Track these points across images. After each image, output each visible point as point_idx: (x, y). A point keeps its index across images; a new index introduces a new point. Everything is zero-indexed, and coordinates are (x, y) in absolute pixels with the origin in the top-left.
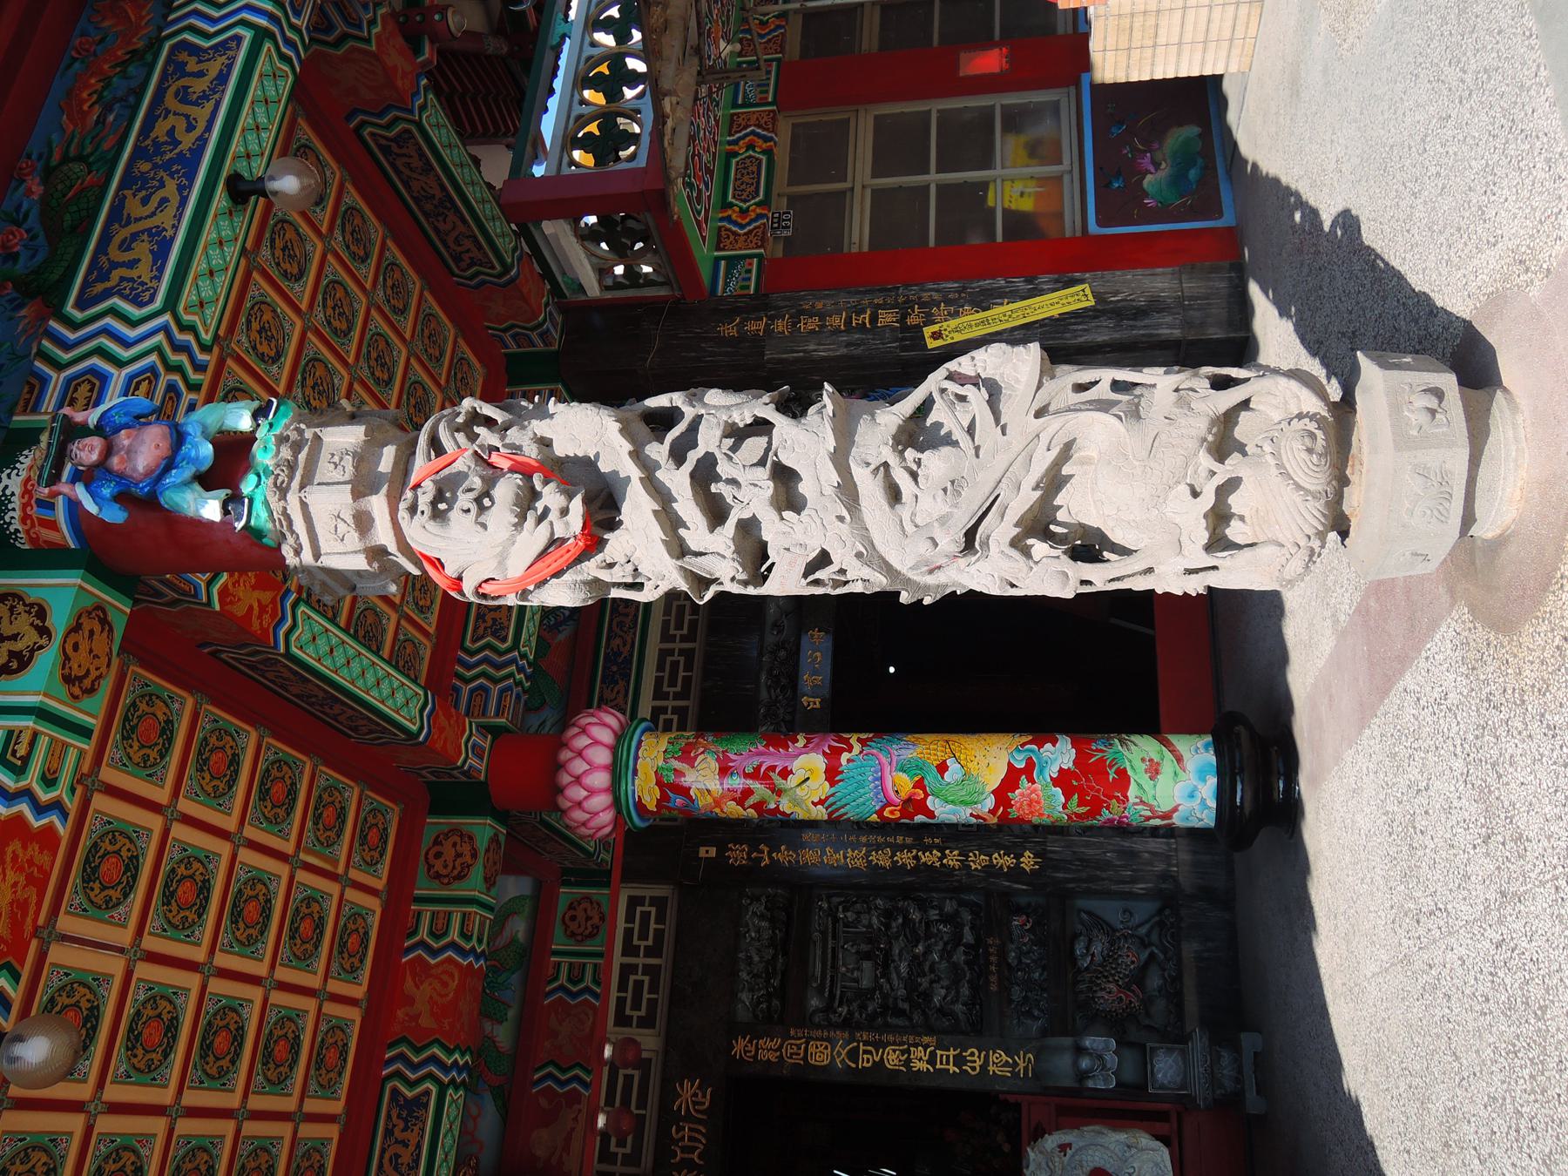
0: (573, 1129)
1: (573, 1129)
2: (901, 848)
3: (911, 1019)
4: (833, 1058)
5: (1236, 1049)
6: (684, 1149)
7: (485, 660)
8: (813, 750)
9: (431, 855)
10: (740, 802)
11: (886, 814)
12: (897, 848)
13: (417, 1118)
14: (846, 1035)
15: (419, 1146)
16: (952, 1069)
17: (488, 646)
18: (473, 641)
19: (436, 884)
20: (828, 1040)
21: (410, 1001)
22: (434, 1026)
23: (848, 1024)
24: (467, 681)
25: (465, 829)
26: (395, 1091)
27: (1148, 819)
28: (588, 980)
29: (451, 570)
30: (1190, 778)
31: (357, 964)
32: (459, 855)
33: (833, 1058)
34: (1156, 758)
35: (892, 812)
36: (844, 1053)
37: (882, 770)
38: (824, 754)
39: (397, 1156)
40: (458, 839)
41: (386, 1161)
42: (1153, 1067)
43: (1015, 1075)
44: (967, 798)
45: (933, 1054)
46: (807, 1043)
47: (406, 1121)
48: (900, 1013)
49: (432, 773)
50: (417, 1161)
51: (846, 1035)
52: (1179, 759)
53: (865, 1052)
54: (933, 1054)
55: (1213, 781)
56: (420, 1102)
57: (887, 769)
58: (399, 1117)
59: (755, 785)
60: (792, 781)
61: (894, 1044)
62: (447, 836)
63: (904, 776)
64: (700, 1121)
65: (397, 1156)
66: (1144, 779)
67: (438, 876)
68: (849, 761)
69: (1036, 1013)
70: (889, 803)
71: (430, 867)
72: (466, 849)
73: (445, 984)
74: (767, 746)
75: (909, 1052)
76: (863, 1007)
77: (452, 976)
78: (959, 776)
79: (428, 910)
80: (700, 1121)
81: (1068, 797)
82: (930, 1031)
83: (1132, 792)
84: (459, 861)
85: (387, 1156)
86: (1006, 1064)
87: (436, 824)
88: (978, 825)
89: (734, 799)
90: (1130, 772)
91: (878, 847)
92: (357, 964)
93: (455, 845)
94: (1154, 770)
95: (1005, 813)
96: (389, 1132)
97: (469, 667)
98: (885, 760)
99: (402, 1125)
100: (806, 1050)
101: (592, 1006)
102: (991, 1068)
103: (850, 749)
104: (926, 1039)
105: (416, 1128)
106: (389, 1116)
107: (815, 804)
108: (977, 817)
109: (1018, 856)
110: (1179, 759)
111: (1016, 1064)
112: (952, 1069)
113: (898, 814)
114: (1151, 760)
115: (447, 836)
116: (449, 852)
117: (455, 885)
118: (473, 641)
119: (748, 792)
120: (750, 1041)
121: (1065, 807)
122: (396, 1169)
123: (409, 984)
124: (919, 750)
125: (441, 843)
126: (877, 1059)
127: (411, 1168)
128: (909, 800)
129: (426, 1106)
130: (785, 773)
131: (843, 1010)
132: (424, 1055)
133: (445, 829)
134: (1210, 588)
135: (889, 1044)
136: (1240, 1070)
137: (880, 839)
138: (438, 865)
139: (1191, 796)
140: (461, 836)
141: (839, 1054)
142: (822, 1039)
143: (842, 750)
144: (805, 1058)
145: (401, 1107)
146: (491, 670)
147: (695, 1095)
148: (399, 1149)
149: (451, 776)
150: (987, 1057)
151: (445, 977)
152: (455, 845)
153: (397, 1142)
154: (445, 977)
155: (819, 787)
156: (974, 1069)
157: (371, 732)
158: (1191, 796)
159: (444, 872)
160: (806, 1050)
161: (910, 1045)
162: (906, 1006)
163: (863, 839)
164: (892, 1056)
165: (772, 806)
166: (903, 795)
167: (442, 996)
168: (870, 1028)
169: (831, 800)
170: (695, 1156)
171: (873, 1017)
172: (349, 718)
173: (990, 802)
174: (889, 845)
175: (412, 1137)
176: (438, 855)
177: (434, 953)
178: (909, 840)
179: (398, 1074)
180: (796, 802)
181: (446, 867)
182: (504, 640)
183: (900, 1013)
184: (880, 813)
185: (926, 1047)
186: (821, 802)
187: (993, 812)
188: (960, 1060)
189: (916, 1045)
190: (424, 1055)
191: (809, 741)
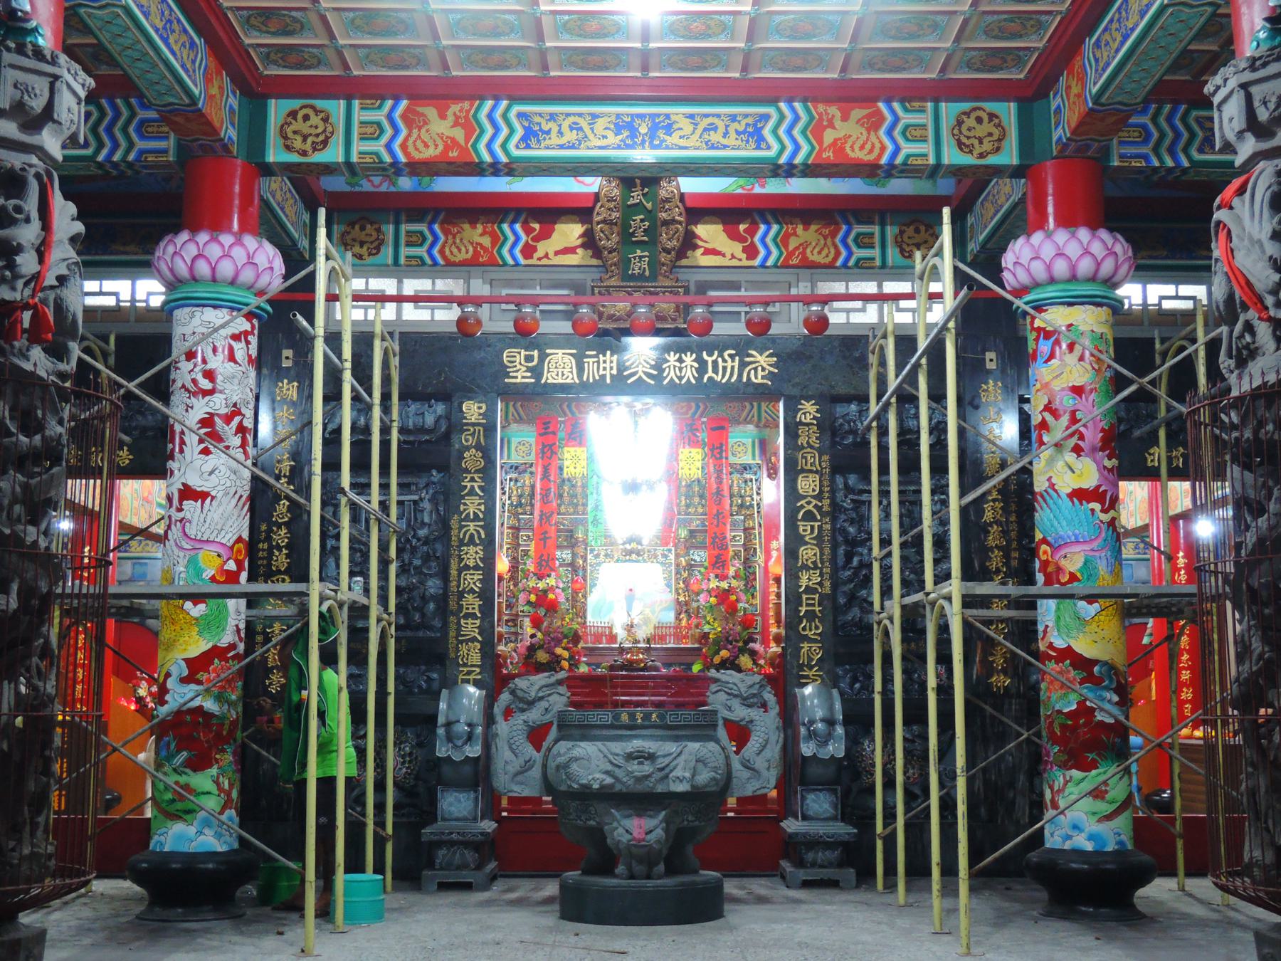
0: (724, 255)
1: (724, 255)
2: (1007, 556)
3: (844, 568)
4: (805, 497)
5: (841, 864)
6: (715, 363)
7: (1178, 135)
8: (1101, 474)
9: (979, 113)
10: (1048, 408)
11: (1044, 547)
12: (1006, 551)
13: (747, 141)
14: (826, 509)
15: (725, 147)
16: (803, 609)
17: (1193, 135)
18: (1197, 120)
19: (953, 122)
20: (821, 492)
21: (845, 118)
22: (825, 145)
23: (836, 508)
24: (1154, 119)
25: (1005, 143)
26: (766, 117)
27: (1051, 787)
28: (859, 253)
29: (1236, 202)
30: (1093, 826)
31: (877, 67)
32: (981, 141)
33: (805, 497)
34: (1108, 797)
35: (1045, 552)
36: (810, 507)
37: (1085, 542)
38: (1098, 487)
39: (715, 129)
40: (995, 137)
41: (710, 120)
42: (820, 790)
43: (801, 667)
44: (1062, 623)
45: (814, 591)
46: (816, 472)
47: (744, 132)
48: (849, 556)
49: (1059, 107)
50: (713, 147)
51: (826, 509)
52: (1109, 817)
53: (812, 527)
54: (814, 591)
55: (1089, 847)
56: (760, 141)
57: (1087, 547)
58: (747, 125)
59: (1065, 420)
60: (1070, 457)
61: (822, 554)
62: (999, 125)
63: (1080, 564)
64: (740, 375)
65: (715, 129)
66: (1087, 786)
67: (960, 123)
68: (1093, 510)
69: (857, 685)
70: (1056, 549)
71: (967, 114)
72: (987, 146)
73: (862, 148)
74: (1103, 430)
75: (816, 568)
76: (852, 522)
77: (871, 151)
78: (1082, 614)
79: (926, 118)
80: (740, 375)
81: (1070, 715)
82: (835, 586)
83: (1076, 774)
84: (976, 142)
85: (716, 120)
86: (810, 659)
87: (1008, 111)
88: (1036, 632)
89: (1050, 402)
90: (1094, 772)
91: (1005, 533)
92: (877, 67)
93: (990, 134)
94: (1097, 794)
95: (1050, 658)
96: (733, 118)
97: (1169, 119)
98: (1095, 545)
99: (741, 129)
100: (811, 471)
101: (835, 259)
102: (805, 645)
103: (1104, 511)
104: (827, 584)
105: (739, 142)
106: (746, 116)
107: (1049, 479)
108: (1045, 632)
109: (1004, 671)
110: (1109, 817)
111: (811, 668)
112: (803, 609)
113: (1044, 558)
114: (1106, 792)
115: (999, 125)
116: (981, 131)
117: (953, 142)
118: (1197, 120)
119: (1055, 414)
120: (814, 418)
121: (1059, 712)
122: (705, 130)
123: (857, 113)
124: (1106, 576)
125: (990, 120)
126: (807, 539)
127: (706, 143)
128: (1059, 569)
129: (758, 148)
130: (1077, 450)
131: (847, 504)
132: (800, 140)
133: (1005, 123)
134: (1069, 647)
135: (821, 550)
136: (822, 866)
137: (1013, 534)
138: (971, 122)
139: (1075, 827)
140: (1000, 140)
141: (809, 503)
142: (821, 486)
143: (1103, 503)
144: (803, 471)
145: (755, 125)
146: (1167, 142)
147: (763, 369)
148: (721, 129)
149: (1057, 125)
150: (815, 641)
151: (868, 147)
152: (990, 134)
153: (727, 126)
154: (868, 147)
155: (1067, 483)
156: (804, 629)
157: (1097, 60)
158: (1075, 827)
159: (905, 237)
160: (811, 471)
161: (821, 569)
162: (855, 561)
163: (1013, 518)
164: (811, 553)
165: (1045, 439)
166: (1063, 563)
167: (852, 147)
168: (833, 530)
169: (1055, 495)
170: (710, 373)
171: (843, 531)
172: (1107, 44)
173: (1060, 643)
174: (1009, 542)
175: (732, 140)
176: (979, 120)
177: (890, 133)
178: (1014, 563)
179: (782, 117)
180: (1051, 461)
181: (969, 129)
182: (1201, 151)
183: (849, 556)
184: (1044, 541)
185: (820, 584)
186: (1052, 486)
187: (1051, 646)
188: (811, 616)
189: (821, 575)
190: (800, 140)
191: (1110, 470)
